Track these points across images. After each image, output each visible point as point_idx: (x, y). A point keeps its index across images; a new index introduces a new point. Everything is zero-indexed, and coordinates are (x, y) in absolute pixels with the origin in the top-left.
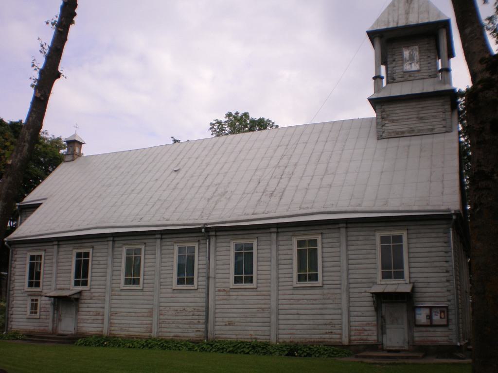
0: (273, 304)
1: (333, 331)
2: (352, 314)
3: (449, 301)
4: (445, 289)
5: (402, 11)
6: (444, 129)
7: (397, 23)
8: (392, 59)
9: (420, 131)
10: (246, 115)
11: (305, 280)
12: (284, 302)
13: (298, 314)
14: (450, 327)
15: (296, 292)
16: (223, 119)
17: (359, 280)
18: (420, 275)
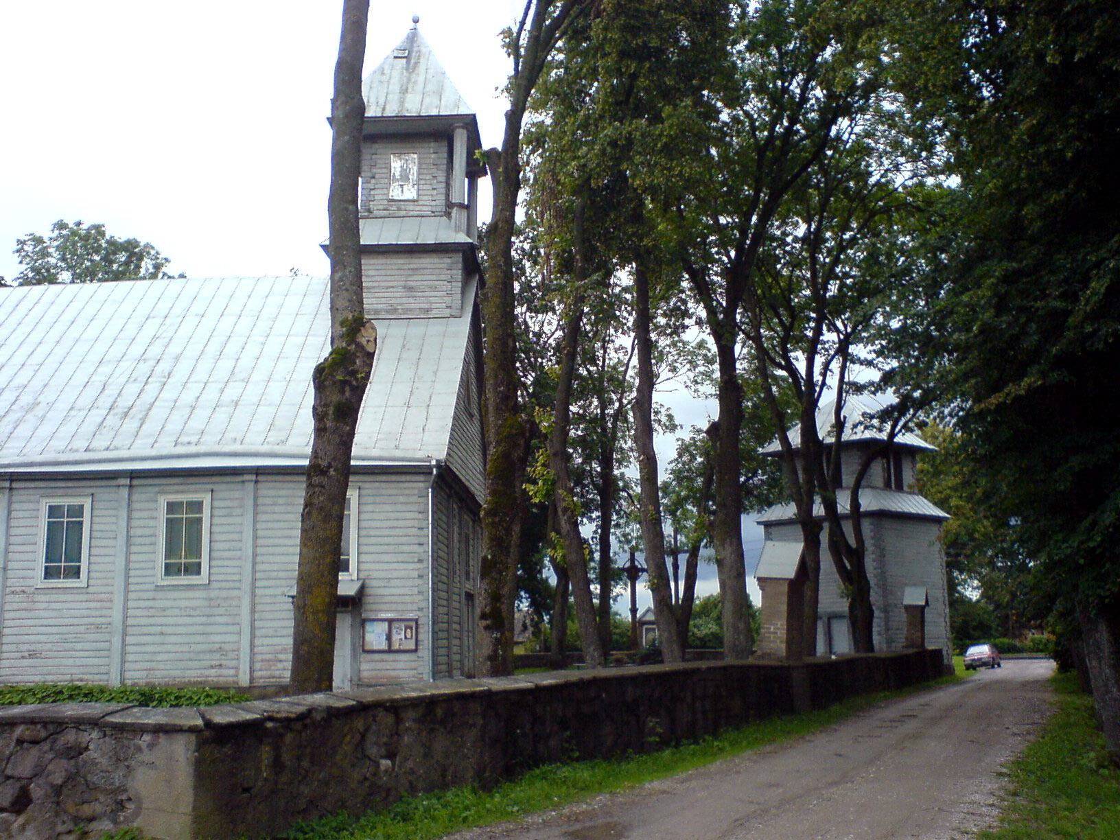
0: (117, 616)
1: (224, 662)
2: (258, 633)
3: (421, 609)
4: (416, 590)
5: (395, 87)
6: (448, 311)
7: (384, 109)
8: (370, 175)
9: (406, 311)
10: (99, 230)
11: (179, 572)
12: (138, 612)
13: (162, 634)
14: (420, 654)
15: (160, 594)
16: (46, 233)
17: (274, 574)
18: (377, 566)
